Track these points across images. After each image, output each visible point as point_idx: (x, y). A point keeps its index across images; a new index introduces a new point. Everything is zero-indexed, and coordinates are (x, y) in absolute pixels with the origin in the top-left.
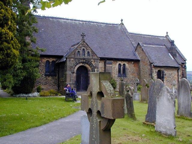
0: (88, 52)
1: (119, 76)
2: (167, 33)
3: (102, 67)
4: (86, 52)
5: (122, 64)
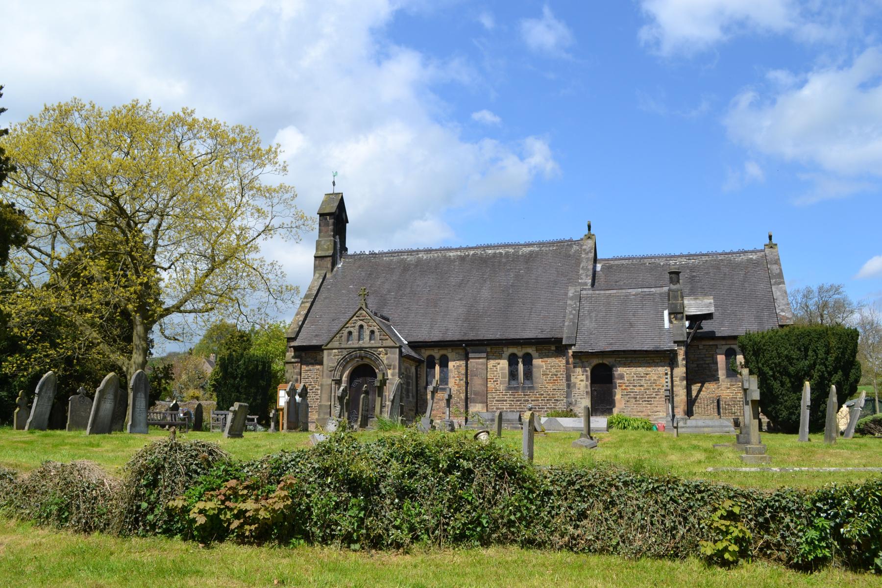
1: (509, 388)
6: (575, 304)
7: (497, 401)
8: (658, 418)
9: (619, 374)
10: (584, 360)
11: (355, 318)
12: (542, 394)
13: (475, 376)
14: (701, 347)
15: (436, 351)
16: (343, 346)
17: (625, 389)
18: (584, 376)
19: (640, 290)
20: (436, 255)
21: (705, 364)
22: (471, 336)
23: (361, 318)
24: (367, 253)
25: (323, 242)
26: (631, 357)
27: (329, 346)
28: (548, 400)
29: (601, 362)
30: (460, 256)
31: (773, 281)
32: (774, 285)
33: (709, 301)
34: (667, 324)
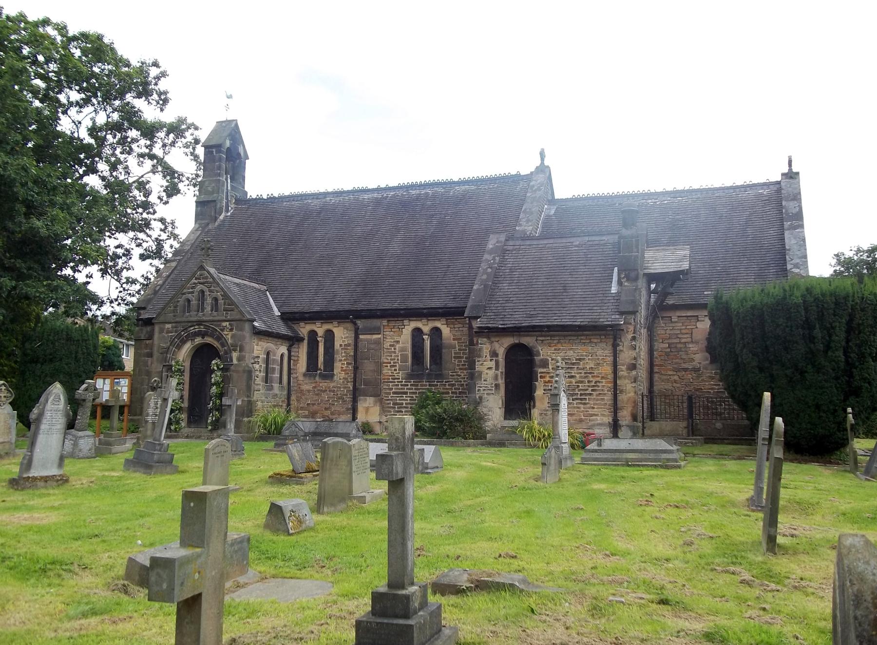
0: (216, 299)
1: (410, 377)
2: (542, 155)
3: (349, 345)
4: (209, 300)
5: (426, 329)
6: (494, 259)
7: (394, 393)
8: (594, 425)
9: (542, 360)
10: (493, 339)
11: (194, 281)
12: (453, 385)
13: (366, 359)
14: (674, 319)
15: (318, 324)
16: (178, 319)
17: (549, 382)
18: (493, 363)
19: (587, 239)
20: (347, 198)
21: (680, 343)
22: (359, 306)
23: (201, 281)
24: (265, 197)
25: (207, 183)
26: (558, 336)
27: (162, 319)
28: (460, 393)
29: (517, 342)
30: (376, 198)
31: (787, 224)
32: (788, 229)
33: (682, 253)
34: (614, 289)
